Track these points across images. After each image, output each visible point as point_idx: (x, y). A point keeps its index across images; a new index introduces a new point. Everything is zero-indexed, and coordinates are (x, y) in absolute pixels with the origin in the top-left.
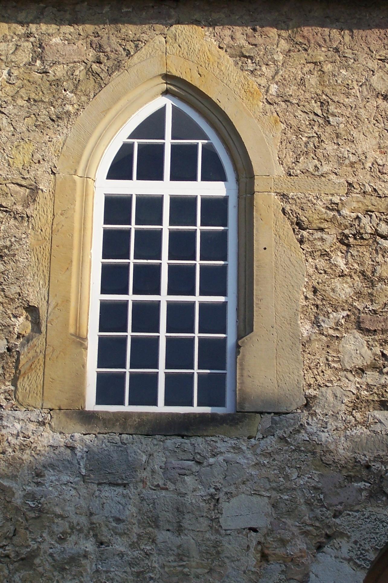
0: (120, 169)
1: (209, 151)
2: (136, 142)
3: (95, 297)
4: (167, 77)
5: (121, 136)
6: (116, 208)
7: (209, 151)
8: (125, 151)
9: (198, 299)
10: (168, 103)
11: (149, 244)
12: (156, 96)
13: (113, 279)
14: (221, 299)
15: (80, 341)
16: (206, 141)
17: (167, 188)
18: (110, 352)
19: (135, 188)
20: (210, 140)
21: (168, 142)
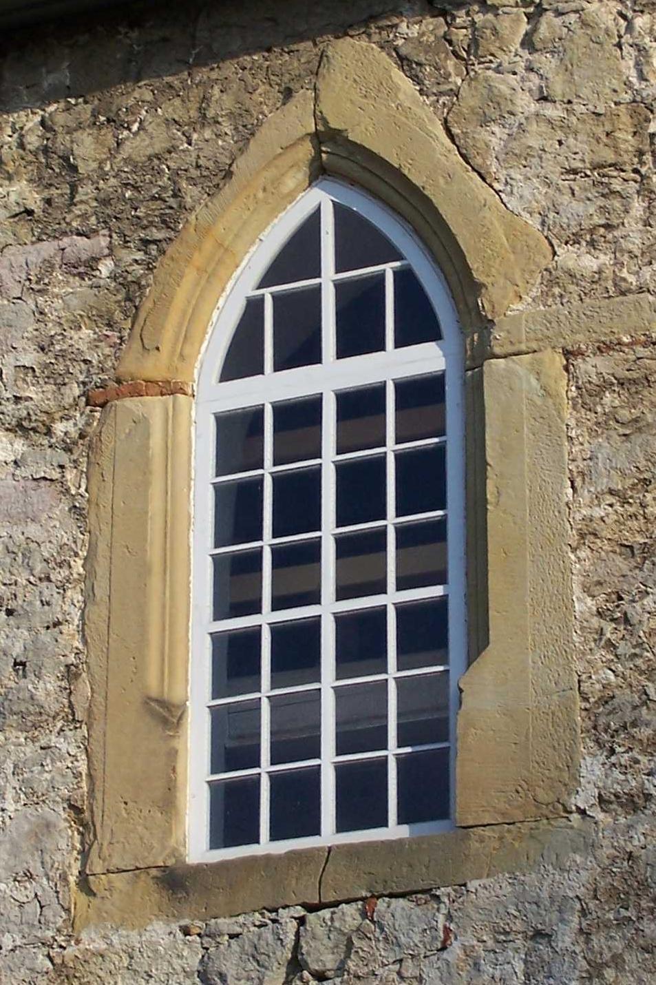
0: (242, 360)
1: (406, 279)
3: (200, 626)
5: (243, 279)
6: (238, 433)
14: (436, 591)
16: (397, 264)
17: (331, 376)
19: (271, 387)
20: (406, 259)
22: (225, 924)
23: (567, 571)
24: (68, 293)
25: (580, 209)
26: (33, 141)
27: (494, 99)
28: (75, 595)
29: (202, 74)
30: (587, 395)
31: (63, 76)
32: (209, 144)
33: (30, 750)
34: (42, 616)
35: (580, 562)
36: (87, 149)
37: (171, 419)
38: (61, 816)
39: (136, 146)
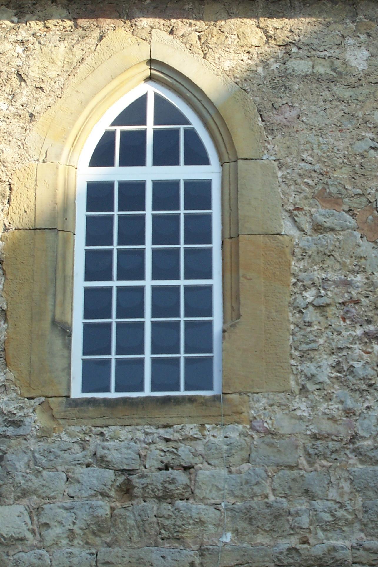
0: (102, 156)
2: (118, 129)
3: (79, 284)
4: (151, 62)
7: (191, 134)
8: (108, 139)
9: (182, 282)
10: (151, 90)
11: (132, 231)
12: (138, 83)
13: (96, 267)
15: (66, 332)
17: (149, 173)
18: (96, 340)
19: (117, 174)
21: (150, 127)
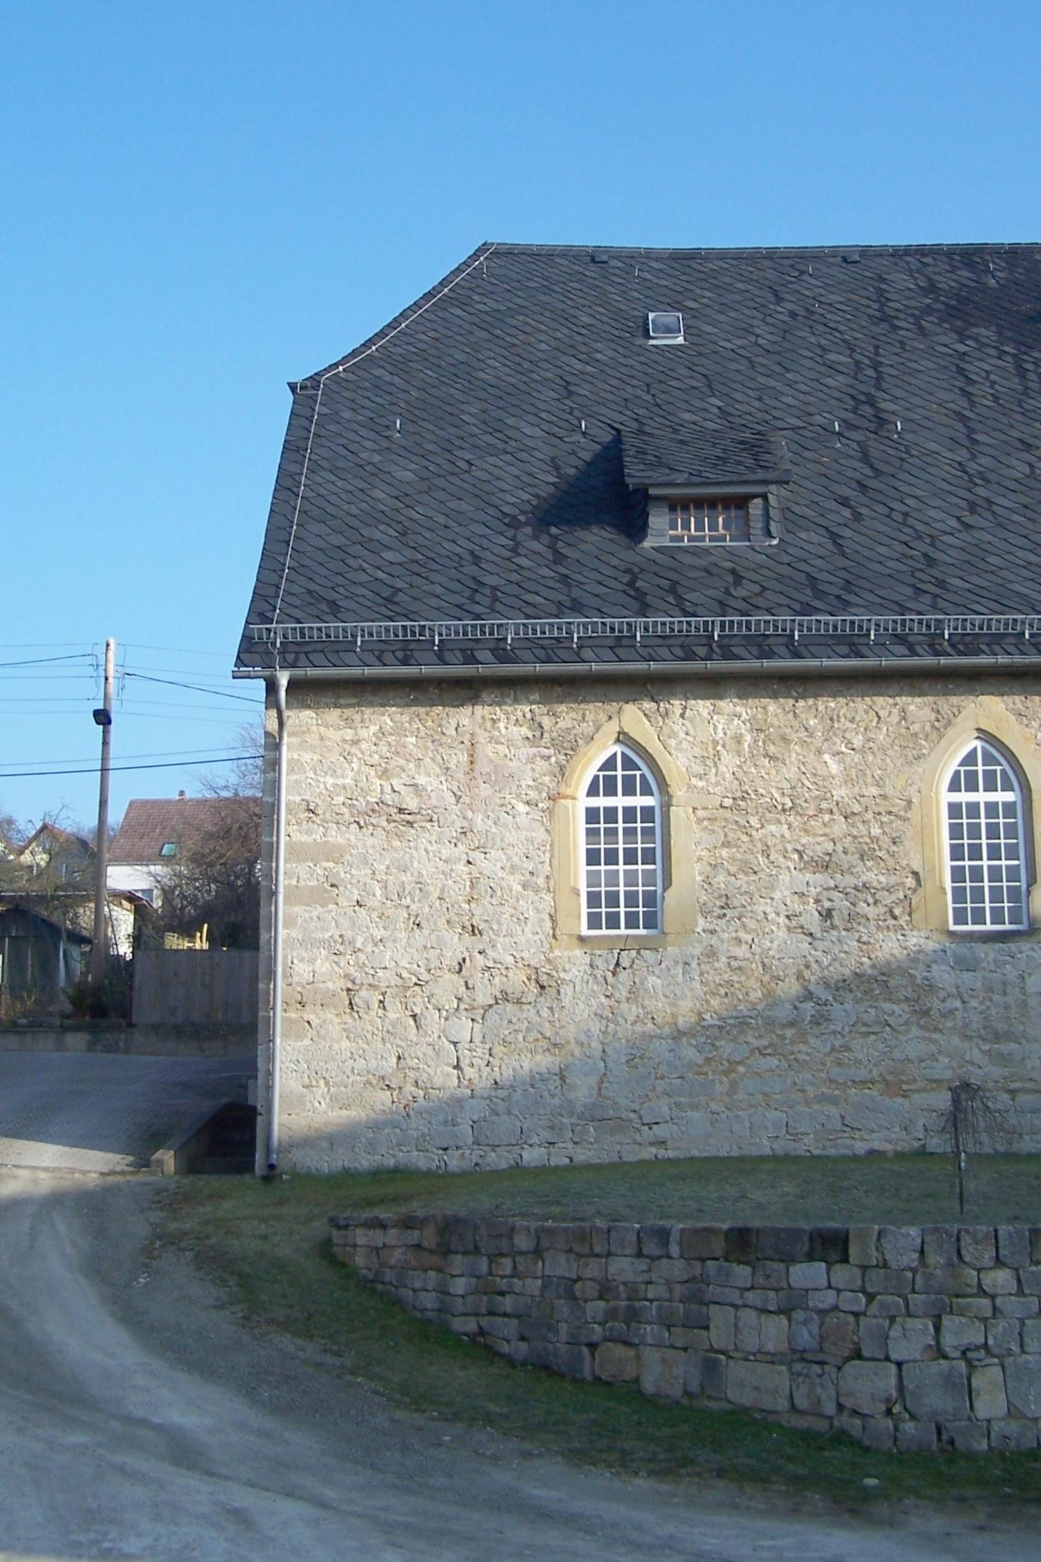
0: (593, 791)
5: (592, 770)
19: (602, 802)
22: (598, 952)
23: (694, 869)
24: (541, 765)
25: (698, 769)
26: (529, 716)
27: (674, 732)
28: (548, 855)
29: (582, 706)
30: (699, 821)
31: (536, 697)
32: (587, 728)
33: (536, 898)
34: (537, 860)
35: (698, 867)
36: (547, 722)
37: (574, 806)
38: (547, 918)
39: (562, 724)
